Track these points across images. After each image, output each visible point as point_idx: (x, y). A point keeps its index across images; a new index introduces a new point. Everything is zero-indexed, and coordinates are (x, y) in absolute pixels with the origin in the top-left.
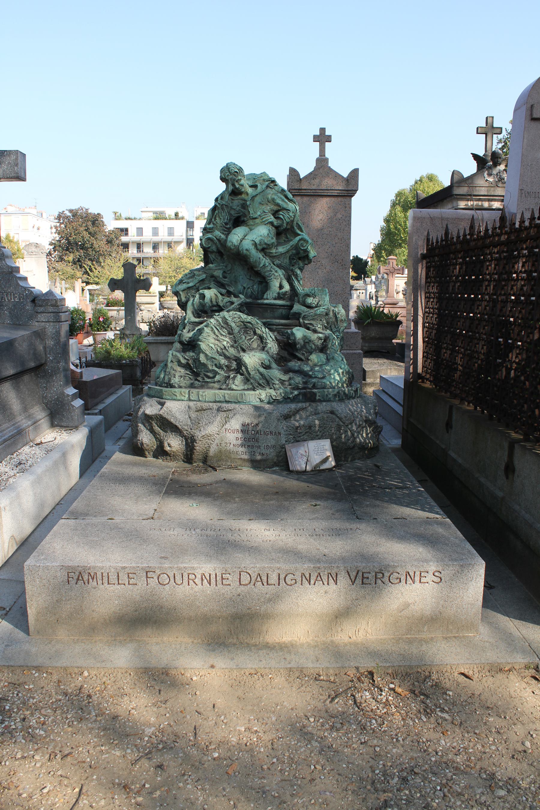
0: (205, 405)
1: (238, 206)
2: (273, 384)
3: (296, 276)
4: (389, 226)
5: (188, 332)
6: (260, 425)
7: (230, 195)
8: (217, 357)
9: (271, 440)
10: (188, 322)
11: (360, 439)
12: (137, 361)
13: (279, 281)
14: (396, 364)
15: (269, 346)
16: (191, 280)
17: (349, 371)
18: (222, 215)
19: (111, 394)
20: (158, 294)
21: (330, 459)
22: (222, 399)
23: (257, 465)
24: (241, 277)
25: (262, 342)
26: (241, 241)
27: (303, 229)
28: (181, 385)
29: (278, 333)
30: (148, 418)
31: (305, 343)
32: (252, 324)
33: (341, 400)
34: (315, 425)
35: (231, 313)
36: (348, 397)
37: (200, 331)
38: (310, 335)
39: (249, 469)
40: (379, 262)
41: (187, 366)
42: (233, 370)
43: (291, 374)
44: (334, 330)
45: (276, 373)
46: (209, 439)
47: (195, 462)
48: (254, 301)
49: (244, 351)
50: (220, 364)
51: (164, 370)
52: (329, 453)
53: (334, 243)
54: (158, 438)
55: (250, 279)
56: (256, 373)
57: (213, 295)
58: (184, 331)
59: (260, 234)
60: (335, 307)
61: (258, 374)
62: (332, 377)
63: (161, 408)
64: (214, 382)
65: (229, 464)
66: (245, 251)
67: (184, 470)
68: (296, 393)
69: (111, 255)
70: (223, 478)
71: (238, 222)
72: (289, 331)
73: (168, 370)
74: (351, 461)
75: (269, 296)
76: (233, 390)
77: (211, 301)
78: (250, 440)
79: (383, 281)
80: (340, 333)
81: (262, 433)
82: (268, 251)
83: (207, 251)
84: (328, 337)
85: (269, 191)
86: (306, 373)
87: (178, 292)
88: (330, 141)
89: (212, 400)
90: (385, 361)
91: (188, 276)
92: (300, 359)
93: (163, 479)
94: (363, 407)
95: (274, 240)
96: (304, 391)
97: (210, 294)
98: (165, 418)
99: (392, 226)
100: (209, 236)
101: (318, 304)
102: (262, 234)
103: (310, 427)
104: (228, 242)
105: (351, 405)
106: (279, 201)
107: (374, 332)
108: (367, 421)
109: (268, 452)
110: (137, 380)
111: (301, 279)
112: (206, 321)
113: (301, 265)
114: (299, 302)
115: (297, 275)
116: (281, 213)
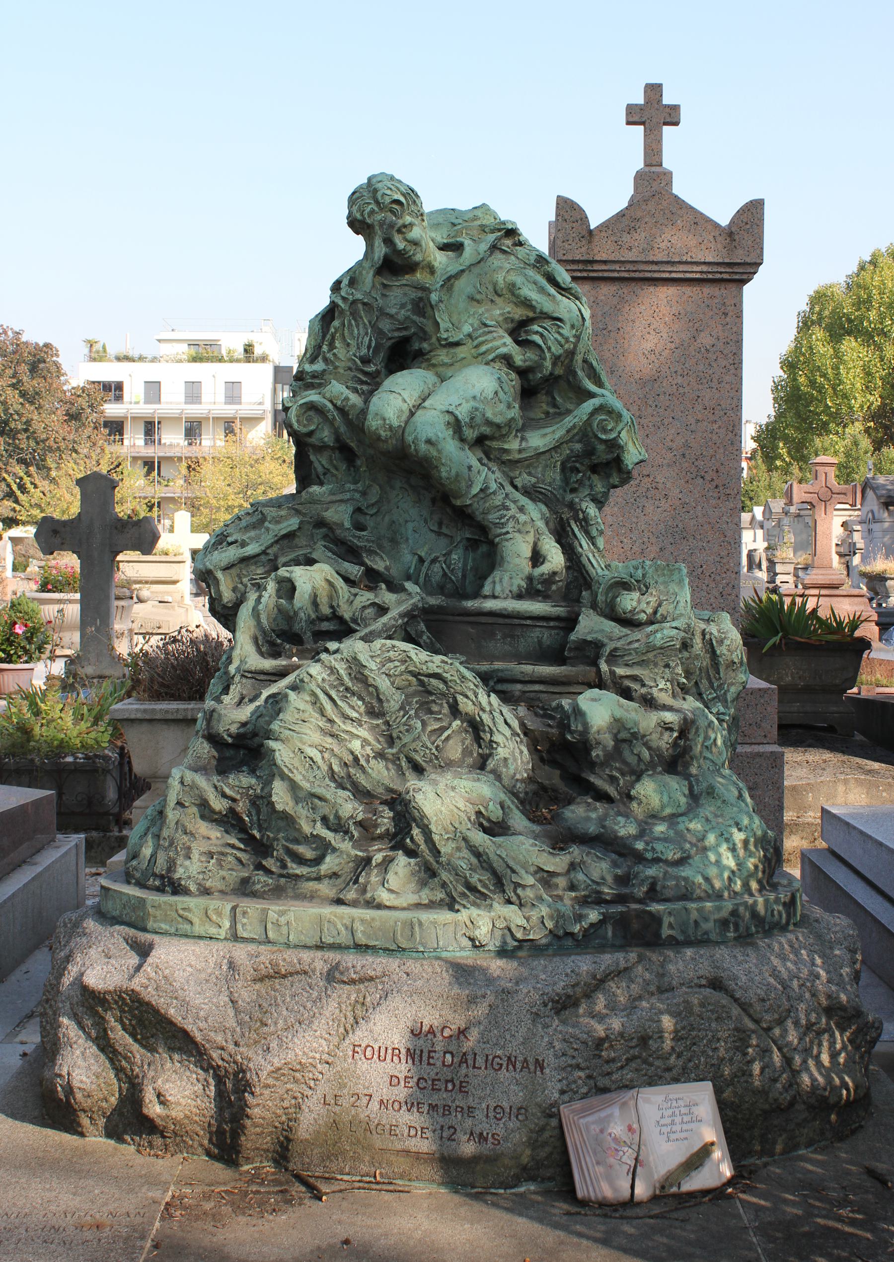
0: (289, 959)
1: (403, 306)
2: (517, 885)
3: (585, 524)
4: (795, 380)
5: (239, 703)
6: (474, 1034)
7: (379, 272)
8: (330, 791)
9: (510, 1089)
10: (238, 669)
11: (811, 1076)
12: (106, 758)
13: (531, 538)
14: (860, 767)
15: (501, 752)
16: (252, 533)
17: (765, 834)
18: (352, 333)
19: (17, 866)
20: (188, 557)
21: (717, 1154)
22: (344, 938)
23: (464, 1175)
24: (410, 526)
25: (478, 739)
26: (412, 414)
27: (604, 377)
28: (208, 884)
29: (530, 707)
30: (92, 1003)
31: (618, 741)
32: (445, 681)
33: (745, 939)
34: (661, 1031)
35: (378, 643)
36: (767, 926)
37: (277, 702)
38: (633, 715)
39: (434, 1188)
40: (770, 470)
41: (229, 821)
42: (380, 837)
43: (575, 852)
44: (709, 695)
45: (525, 849)
46: (296, 1081)
47: (248, 1160)
48: (452, 603)
49: (418, 770)
50: (338, 817)
51: (154, 830)
52: (710, 1132)
53: (693, 421)
54: (122, 1069)
55: (439, 534)
56: (458, 849)
57: (321, 584)
58: (226, 699)
59: (471, 392)
60: (708, 621)
61: (465, 853)
62: (712, 857)
63: (138, 968)
64: (318, 879)
65: (364, 1169)
66: (423, 447)
67: (207, 1197)
68: (593, 916)
69: (76, 452)
70: (342, 1232)
71: (401, 354)
72: (566, 703)
73: (165, 833)
74: (784, 1152)
75: (498, 588)
76: (380, 906)
77: (315, 603)
78: (440, 1085)
79: (786, 521)
80: (726, 707)
81: (480, 1061)
82: (495, 444)
83: (307, 445)
84: (693, 722)
85: (498, 260)
86: (625, 846)
87: (209, 572)
88: (676, 124)
89: (311, 942)
90: (827, 755)
91: (243, 523)
92: (602, 797)
93: (127, 1239)
94: (818, 961)
95: (515, 412)
96: (620, 908)
97: (313, 579)
98: (148, 1004)
99: (802, 380)
100: (313, 396)
101: (655, 612)
102: (476, 391)
103: (644, 1040)
104: (370, 417)
105: (778, 956)
106: (529, 292)
107: (792, 670)
108: (833, 1010)
109: (500, 1131)
110: (107, 814)
111: (601, 533)
112: (298, 667)
113: (600, 488)
114: (594, 606)
115: (586, 519)
116: (536, 328)
